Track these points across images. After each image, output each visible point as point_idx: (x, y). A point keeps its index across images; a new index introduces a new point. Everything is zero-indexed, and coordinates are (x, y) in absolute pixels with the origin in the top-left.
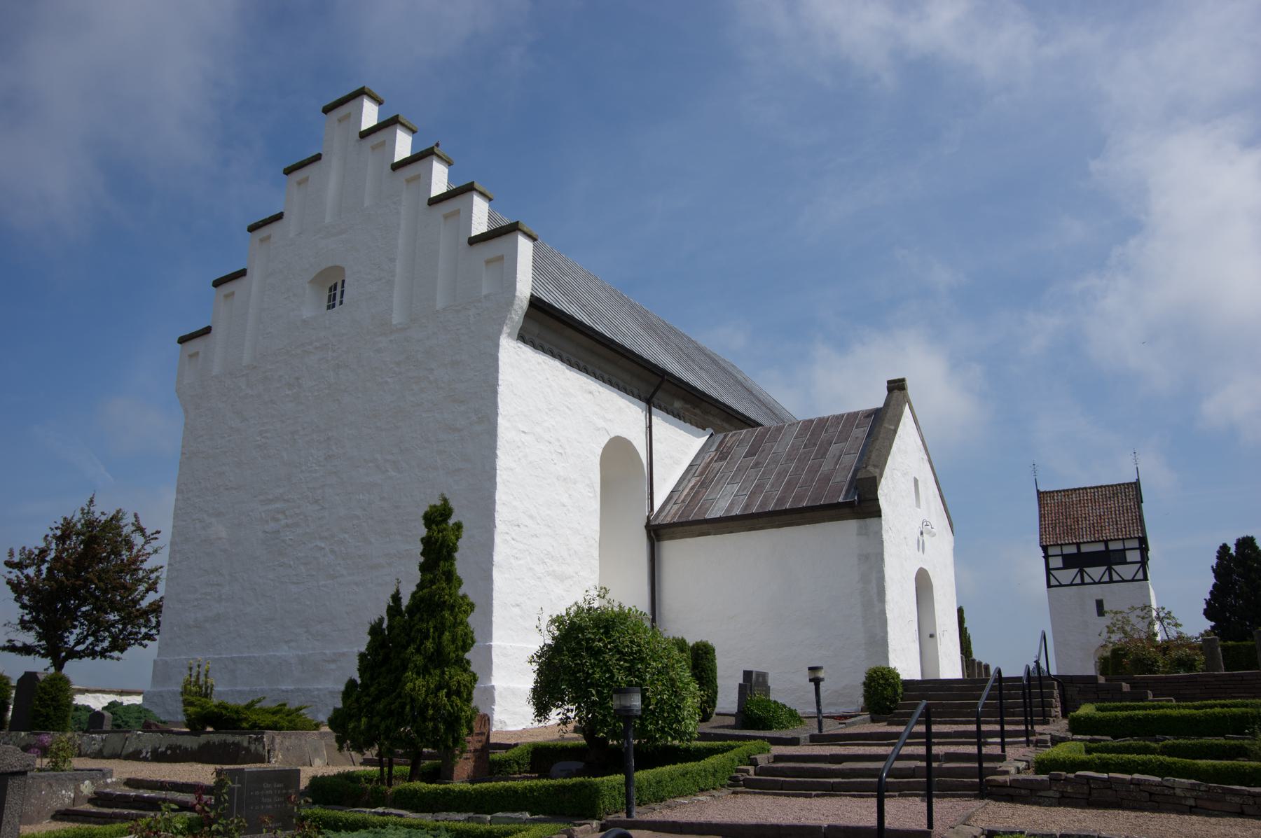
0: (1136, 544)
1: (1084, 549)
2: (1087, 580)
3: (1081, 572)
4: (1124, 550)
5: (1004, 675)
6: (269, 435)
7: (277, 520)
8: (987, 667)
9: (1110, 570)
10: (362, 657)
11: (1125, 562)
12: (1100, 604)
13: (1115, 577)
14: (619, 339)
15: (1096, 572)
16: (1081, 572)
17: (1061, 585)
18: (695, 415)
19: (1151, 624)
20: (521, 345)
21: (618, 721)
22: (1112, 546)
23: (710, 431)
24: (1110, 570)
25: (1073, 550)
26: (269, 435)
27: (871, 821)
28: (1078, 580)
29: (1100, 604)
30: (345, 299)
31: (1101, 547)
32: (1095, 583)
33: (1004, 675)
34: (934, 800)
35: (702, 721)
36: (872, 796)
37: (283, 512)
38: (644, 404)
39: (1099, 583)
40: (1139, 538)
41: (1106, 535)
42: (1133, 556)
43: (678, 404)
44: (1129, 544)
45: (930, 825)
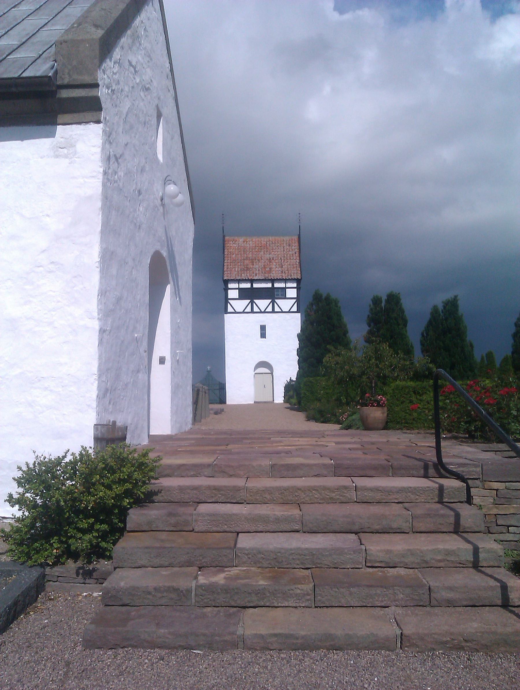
0: (295, 285)
1: (255, 286)
2: (256, 309)
3: (252, 303)
4: (286, 288)
9: (273, 302)
10: (298, 335)
11: (285, 298)
12: (263, 328)
13: (277, 309)
15: (263, 303)
16: (252, 303)
17: (282, 312)
21: (70, 475)
22: (276, 285)
24: (273, 302)
25: (248, 285)
28: (249, 309)
29: (263, 328)
31: (269, 285)
32: (261, 312)
35: (404, 402)
36: (432, 434)
39: (265, 312)
41: (274, 275)
44: (289, 285)
45: (129, 532)
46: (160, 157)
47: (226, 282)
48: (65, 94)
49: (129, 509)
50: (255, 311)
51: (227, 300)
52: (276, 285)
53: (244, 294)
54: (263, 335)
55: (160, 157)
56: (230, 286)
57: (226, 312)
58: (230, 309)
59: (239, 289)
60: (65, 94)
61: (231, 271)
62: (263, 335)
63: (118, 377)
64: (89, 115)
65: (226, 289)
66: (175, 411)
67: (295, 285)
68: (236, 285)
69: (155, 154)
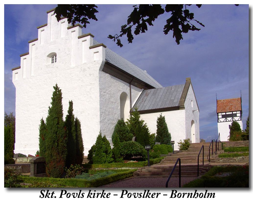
0: (239, 112)
1: (227, 113)
2: (227, 120)
3: (226, 119)
4: (237, 113)
5: (121, 31)
6: (39, 93)
7: (43, 112)
8: (59, 88)
14: (99, 47)
16: (226, 119)
17: (221, 122)
18: (140, 86)
19: (147, 159)
20: (103, 72)
22: (234, 113)
23: (143, 89)
25: (224, 114)
26: (39, 93)
27: (232, 113)
28: (225, 121)
30: (57, 60)
32: (229, 121)
33: (121, 31)
34: (181, 177)
37: (45, 110)
38: (129, 84)
40: (240, 111)
42: (239, 115)
43: (136, 84)
44: (238, 112)
46: (192, 107)
47: (218, 113)
48: (181, 107)
49: (190, 29)
50: (227, 121)
51: (218, 119)
52: (234, 113)
53: (223, 116)
54: (17, 73)
55: (192, 107)
56: (219, 114)
57: (218, 122)
58: (219, 121)
59: (222, 115)
60: (181, 107)
61: (219, 110)
62: (17, 73)
63: (188, 136)
64: (183, 109)
65: (218, 115)
66: (196, 139)
67: (239, 112)
68: (221, 114)
69: (191, 106)
